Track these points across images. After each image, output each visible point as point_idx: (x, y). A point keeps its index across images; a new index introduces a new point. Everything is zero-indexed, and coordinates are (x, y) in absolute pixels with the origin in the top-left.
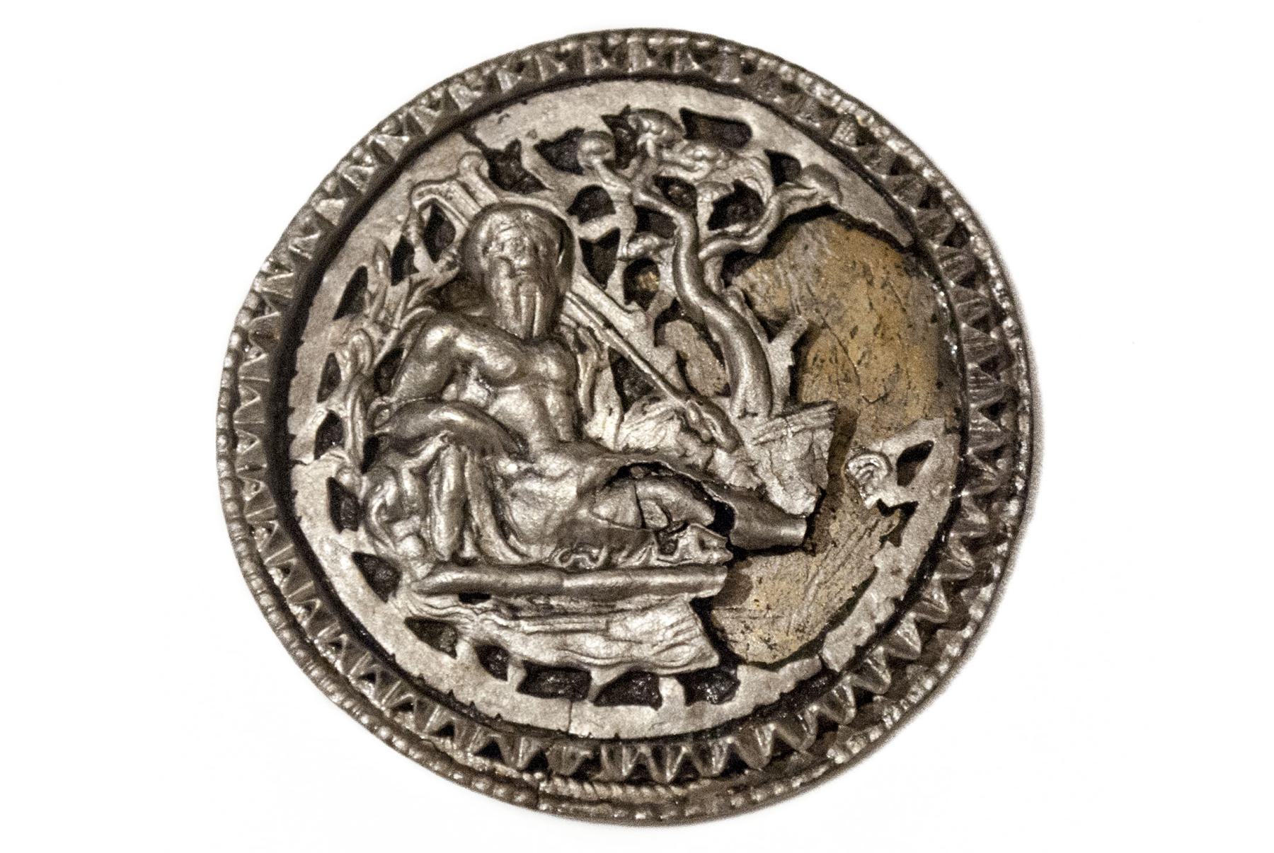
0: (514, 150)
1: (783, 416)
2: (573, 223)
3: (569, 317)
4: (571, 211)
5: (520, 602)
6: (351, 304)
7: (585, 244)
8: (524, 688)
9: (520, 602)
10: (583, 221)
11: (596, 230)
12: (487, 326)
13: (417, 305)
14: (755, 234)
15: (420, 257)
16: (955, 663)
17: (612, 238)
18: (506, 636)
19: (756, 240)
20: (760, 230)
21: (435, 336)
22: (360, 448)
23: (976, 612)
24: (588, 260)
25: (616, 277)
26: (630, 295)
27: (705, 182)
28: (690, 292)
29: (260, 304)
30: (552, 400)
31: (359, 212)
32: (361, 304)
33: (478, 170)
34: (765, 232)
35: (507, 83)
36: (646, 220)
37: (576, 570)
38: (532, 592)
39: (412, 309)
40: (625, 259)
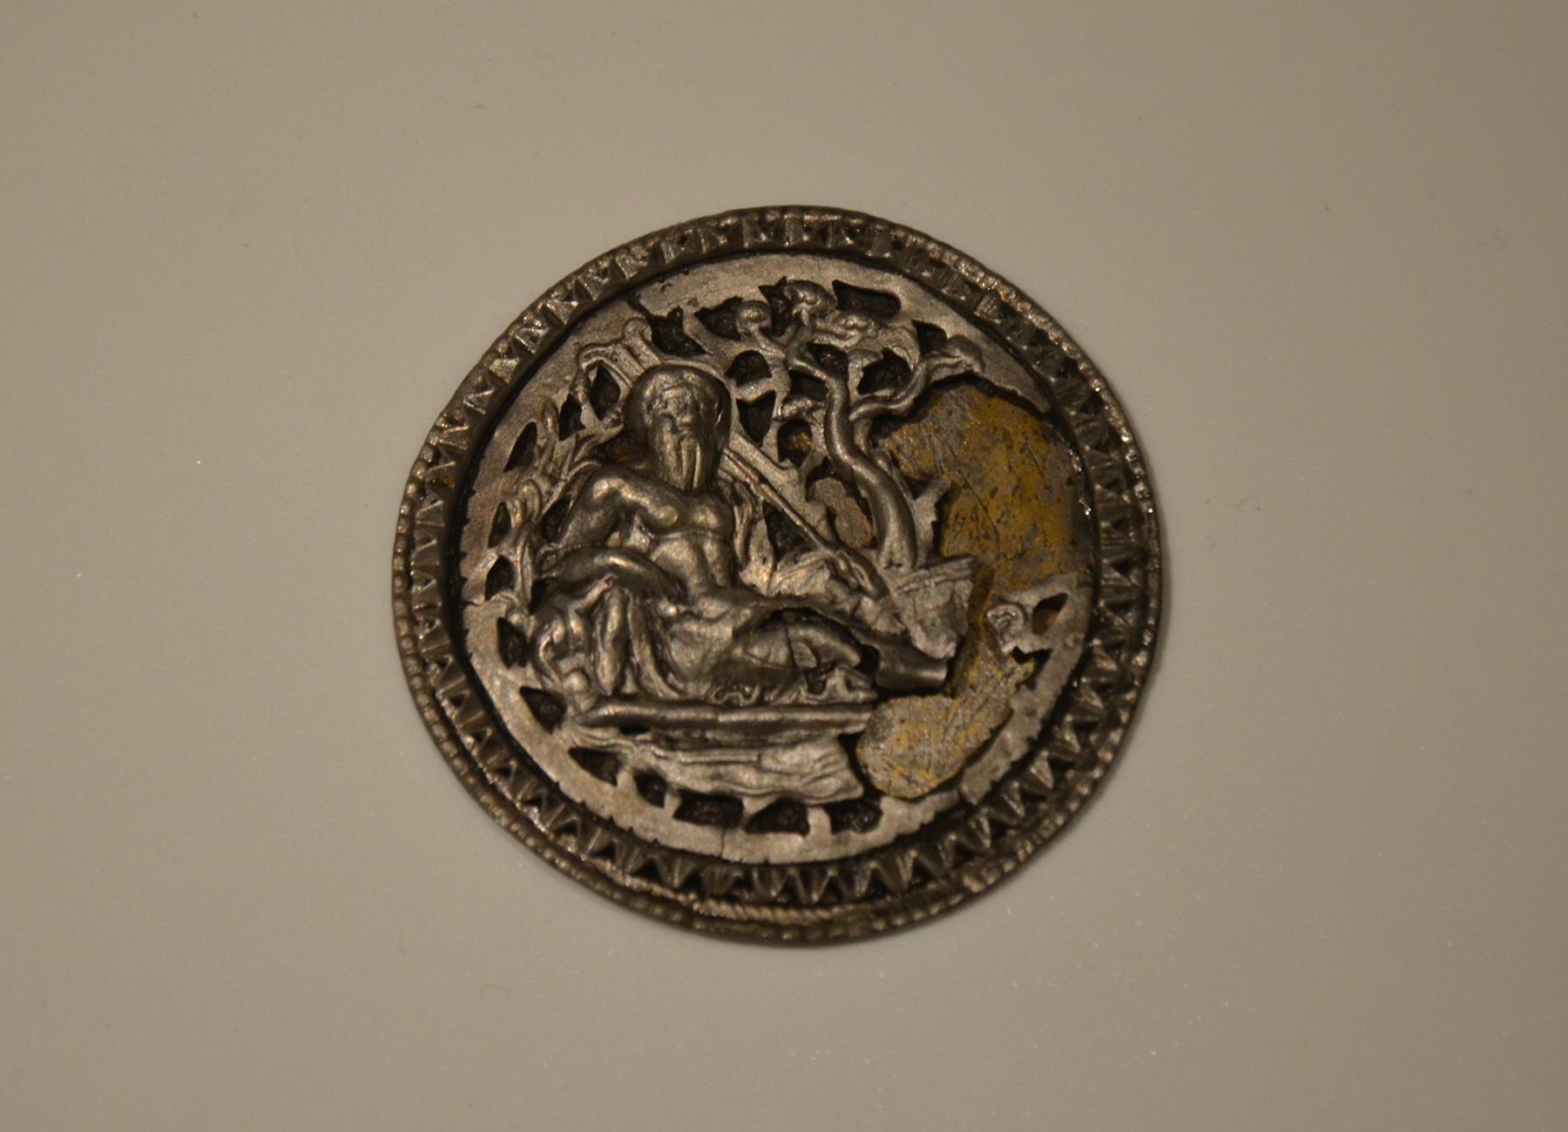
5: (677, 734)
9: (677, 734)
10: (741, 383)
11: (752, 393)
13: (583, 459)
14: (903, 399)
15: (587, 415)
17: (769, 398)
25: (771, 437)
35: (670, 255)
36: (800, 384)
40: (782, 419)
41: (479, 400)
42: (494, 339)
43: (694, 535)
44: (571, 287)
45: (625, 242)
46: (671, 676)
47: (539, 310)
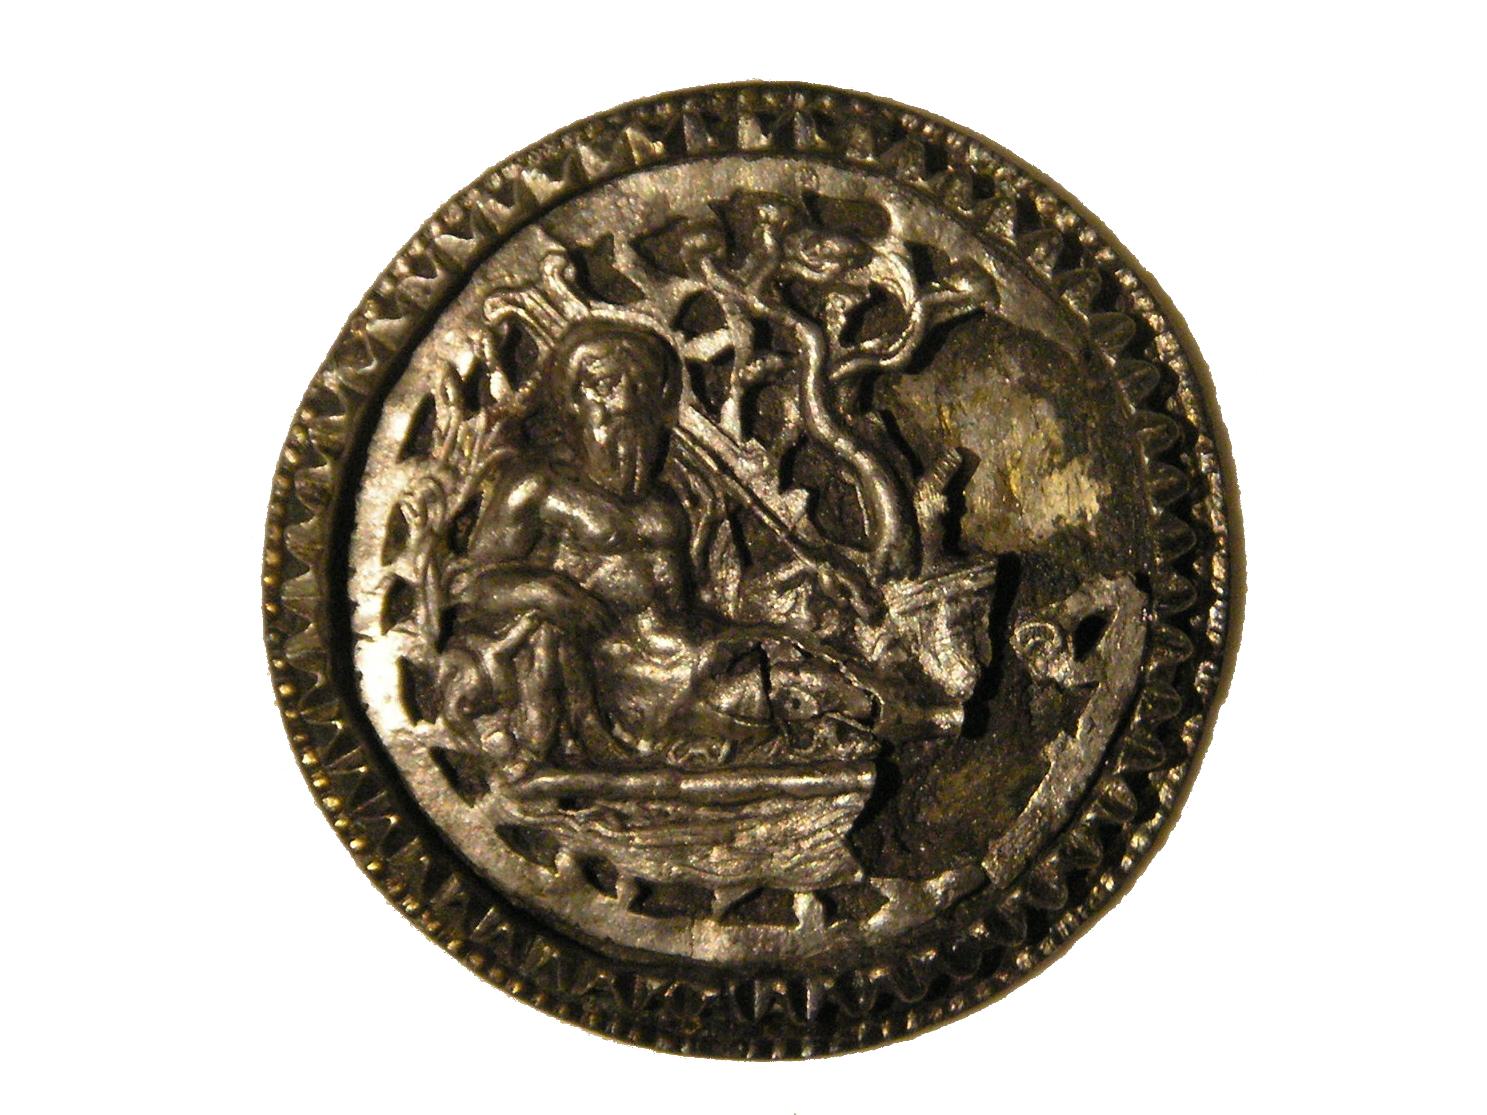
0: (605, 244)
1: (932, 577)
2: (676, 339)
3: (684, 430)
4: (677, 324)
5: (630, 808)
6: (415, 447)
7: (695, 366)
8: (636, 906)
9: (630, 808)
10: (691, 335)
11: (706, 347)
12: (576, 482)
13: (495, 446)
14: (896, 352)
15: (497, 384)
16: (1142, 858)
17: (726, 356)
18: (615, 851)
19: (896, 359)
20: (902, 346)
21: (518, 496)
22: (435, 620)
23: (1164, 794)
24: (698, 387)
25: (730, 408)
26: (749, 428)
27: (836, 284)
28: (823, 428)
29: (318, 401)
30: (661, 566)
31: (423, 326)
32: (429, 443)
33: (562, 275)
34: (911, 344)
35: (589, 158)
36: (764, 335)
37: (695, 770)
38: (642, 797)
39: (489, 452)
40: (742, 383)
41: (362, 377)
42: (502, 158)
43: (628, 544)
44: (459, 215)
45: (493, 163)
46: (618, 729)
47: (380, 301)
